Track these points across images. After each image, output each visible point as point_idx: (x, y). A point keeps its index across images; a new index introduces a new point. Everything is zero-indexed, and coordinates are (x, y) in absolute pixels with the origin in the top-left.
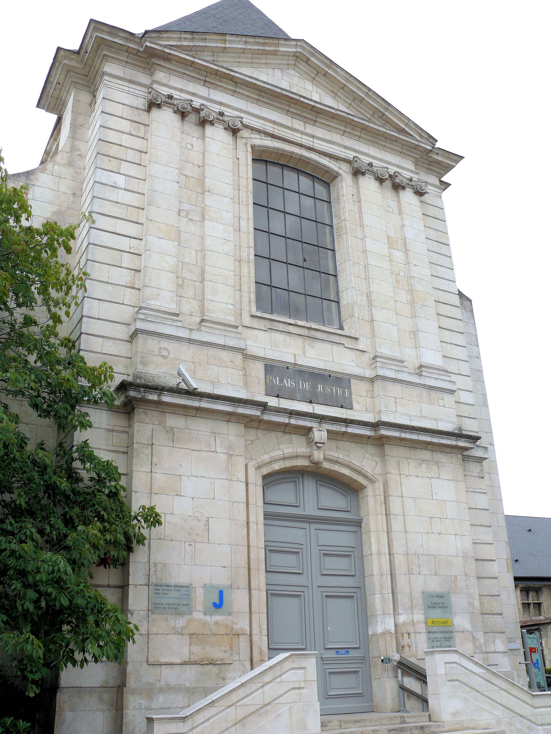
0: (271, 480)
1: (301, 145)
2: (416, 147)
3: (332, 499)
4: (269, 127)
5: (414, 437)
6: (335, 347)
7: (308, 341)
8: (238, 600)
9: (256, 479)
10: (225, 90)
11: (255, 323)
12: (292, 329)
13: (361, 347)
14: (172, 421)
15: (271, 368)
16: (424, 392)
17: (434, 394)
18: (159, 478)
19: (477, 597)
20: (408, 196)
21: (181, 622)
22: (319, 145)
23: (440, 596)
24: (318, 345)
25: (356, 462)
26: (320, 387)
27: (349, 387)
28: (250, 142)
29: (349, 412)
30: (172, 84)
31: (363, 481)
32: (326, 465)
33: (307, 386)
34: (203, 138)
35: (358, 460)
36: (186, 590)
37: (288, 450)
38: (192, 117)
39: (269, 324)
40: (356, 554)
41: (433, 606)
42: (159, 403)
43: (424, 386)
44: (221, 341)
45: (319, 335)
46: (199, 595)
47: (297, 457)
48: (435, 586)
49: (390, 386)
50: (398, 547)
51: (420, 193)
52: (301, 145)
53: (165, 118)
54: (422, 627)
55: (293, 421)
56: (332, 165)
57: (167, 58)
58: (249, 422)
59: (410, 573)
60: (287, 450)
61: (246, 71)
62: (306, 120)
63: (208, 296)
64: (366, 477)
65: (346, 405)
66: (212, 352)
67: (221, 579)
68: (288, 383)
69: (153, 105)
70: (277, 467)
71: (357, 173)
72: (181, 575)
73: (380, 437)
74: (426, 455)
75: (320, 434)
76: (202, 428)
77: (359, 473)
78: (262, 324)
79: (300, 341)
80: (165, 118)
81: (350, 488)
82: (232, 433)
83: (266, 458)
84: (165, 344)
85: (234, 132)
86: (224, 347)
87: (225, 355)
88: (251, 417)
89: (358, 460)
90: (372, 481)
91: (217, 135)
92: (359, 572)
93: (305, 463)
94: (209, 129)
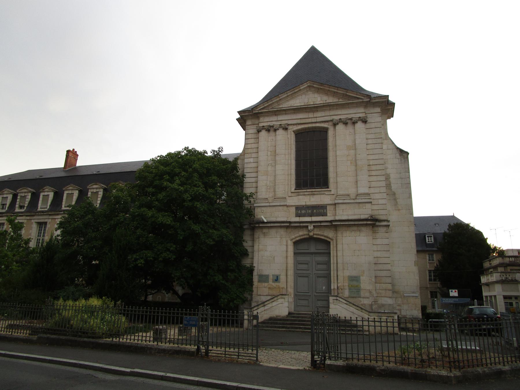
0: (296, 243)
1: (312, 123)
2: (363, 102)
3: (321, 248)
4: (299, 121)
5: (344, 223)
6: (322, 196)
7: (311, 196)
8: (283, 278)
9: (290, 243)
10: (282, 114)
11: (293, 195)
12: (306, 193)
13: (332, 193)
14: (265, 230)
15: (298, 208)
16: (357, 205)
17: (361, 205)
18: (261, 247)
19: (374, 277)
20: (360, 125)
21: (266, 284)
22: (319, 120)
23: (355, 277)
24: (315, 196)
25: (325, 234)
26: (315, 211)
27: (326, 209)
28: (293, 130)
29: (325, 217)
30: (265, 121)
31: (329, 240)
32: (315, 236)
33: (310, 211)
34: (276, 135)
35: (329, 234)
36: (267, 276)
37: (301, 233)
38: (272, 129)
39: (297, 194)
40: (328, 263)
41: (352, 280)
42: (259, 227)
43: (356, 203)
44: (279, 204)
45: (316, 193)
46: (271, 277)
47: (304, 235)
48: (354, 274)
49: (340, 205)
50: (340, 261)
51: (365, 121)
52: (312, 123)
53: (263, 133)
54: (347, 288)
55: (301, 225)
56: (323, 125)
57: (262, 113)
58: (287, 227)
59: (343, 269)
60: (301, 234)
61: (286, 105)
62: (313, 112)
63: (276, 190)
64: (330, 238)
65: (325, 215)
66: (276, 208)
67: (277, 273)
68: (303, 212)
69: (259, 131)
70: (298, 239)
71: (335, 125)
72: (266, 272)
73: (335, 225)
74: (355, 228)
75: (311, 227)
76: (273, 231)
77: (327, 237)
78: (295, 194)
79: (308, 197)
80: (263, 133)
81: (327, 243)
82: (282, 231)
83: (293, 237)
84: (263, 209)
85: (286, 129)
86: (280, 206)
87: (281, 208)
88: (288, 226)
89: (329, 234)
90: (332, 240)
91: (280, 132)
92: (329, 269)
93: (307, 236)
94: (278, 132)
